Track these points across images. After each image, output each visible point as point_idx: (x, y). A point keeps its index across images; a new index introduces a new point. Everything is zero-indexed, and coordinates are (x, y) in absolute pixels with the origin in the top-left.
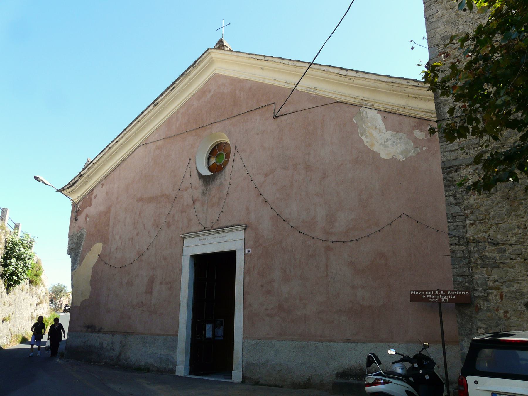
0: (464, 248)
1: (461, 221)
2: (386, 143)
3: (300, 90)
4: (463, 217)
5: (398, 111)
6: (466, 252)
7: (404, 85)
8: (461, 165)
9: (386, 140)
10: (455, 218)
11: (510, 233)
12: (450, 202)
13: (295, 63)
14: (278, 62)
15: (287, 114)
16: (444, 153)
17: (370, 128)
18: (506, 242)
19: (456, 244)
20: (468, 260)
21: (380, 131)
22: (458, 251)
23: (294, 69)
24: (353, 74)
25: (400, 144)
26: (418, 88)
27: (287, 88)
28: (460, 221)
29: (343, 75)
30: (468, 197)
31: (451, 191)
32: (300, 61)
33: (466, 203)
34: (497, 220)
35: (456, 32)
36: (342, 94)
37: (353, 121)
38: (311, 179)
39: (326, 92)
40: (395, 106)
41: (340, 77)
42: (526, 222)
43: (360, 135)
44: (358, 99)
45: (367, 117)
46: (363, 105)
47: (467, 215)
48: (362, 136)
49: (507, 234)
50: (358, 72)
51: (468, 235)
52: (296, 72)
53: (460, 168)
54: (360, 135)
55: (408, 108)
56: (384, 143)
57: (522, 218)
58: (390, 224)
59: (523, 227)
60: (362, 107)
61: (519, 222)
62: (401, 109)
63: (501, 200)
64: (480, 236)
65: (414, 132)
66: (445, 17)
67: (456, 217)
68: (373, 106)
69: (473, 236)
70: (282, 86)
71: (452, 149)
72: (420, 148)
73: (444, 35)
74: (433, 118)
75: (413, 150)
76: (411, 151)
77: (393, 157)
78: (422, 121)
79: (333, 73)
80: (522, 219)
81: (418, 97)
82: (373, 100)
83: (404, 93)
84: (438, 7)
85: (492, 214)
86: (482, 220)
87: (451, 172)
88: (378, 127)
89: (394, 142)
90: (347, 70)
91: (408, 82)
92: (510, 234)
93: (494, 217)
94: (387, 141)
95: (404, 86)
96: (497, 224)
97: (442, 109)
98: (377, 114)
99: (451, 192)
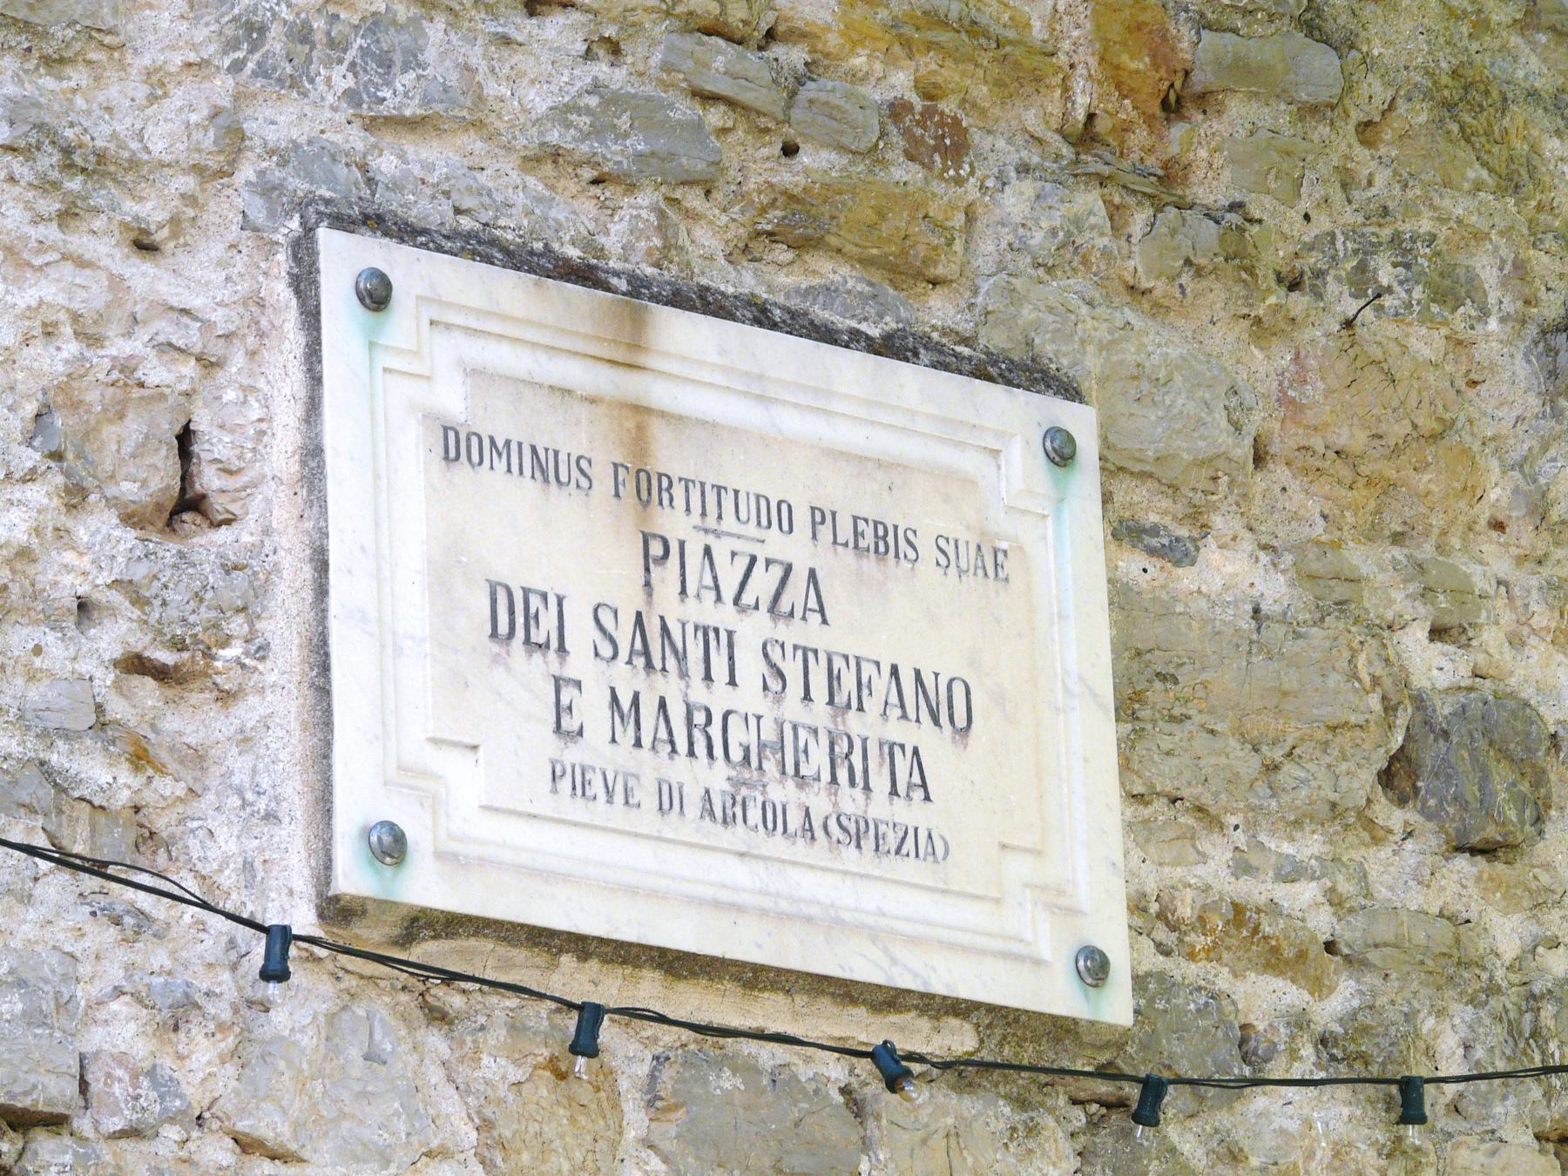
42: (209, 364)
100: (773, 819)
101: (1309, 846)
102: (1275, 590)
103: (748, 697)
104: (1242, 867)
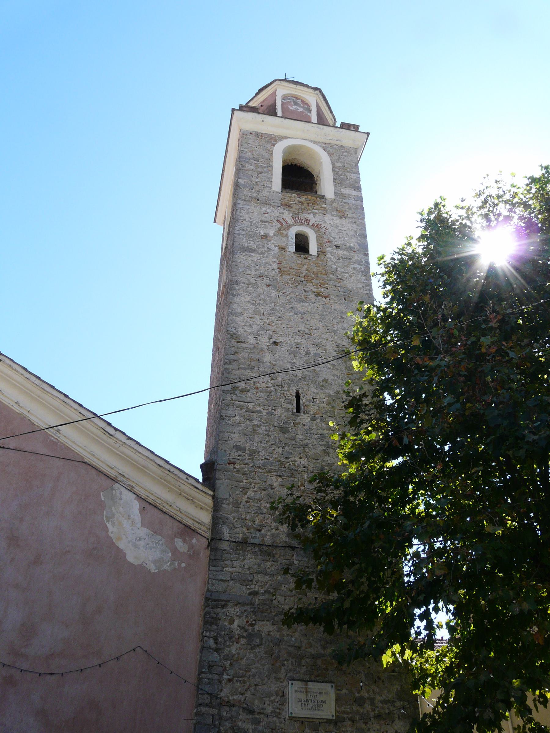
0: (215, 711)
1: (218, 674)
2: (138, 543)
3: (35, 423)
4: (221, 669)
5: (162, 507)
6: (217, 717)
7: (182, 479)
8: (229, 601)
9: (138, 539)
10: (211, 667)
11: (268, 699)
12: (210, 645)
13: (45, 386)
14: (17, 372)
15: (4, 448)
16: (214, 581)
17: (121, 514)
18: (262, 711)
19: (207, 705)
20: (217, 730)
21: (133, 523)
22: (207, 715)
23: (39, 392)
24: (124, 439)
25: (155, 550)
26: (196, 490)
27: (15, 411)
28: (216, 674)
29: (109, 434)
30: (231, 644)
31: (212, 631)
32: (53, 387)
33: (226, 651)
34: (257, 680)
35: (250, 447)
36: (96, 456)
37: (100, 496)
38: (12, 560)
39: (73, 442)
40: (160, 499)
41: (102, 434)
42: (285, 688)
43: (105, 519)
44: (115, 470)
45: (121, 499)
46: (119, 481)
47: (225, 667)
48: (108, 521)
49: (265, 701)
50: (129, 438)
51: (222, 694)
52: (39, 397)
53: (227, 605)
54: (105, 519)
55: (175, 507)
56: (135, 541)
57: (282, 682)
58: (118, 658)
59: (281, 694)
60: (117, 483)
61: (278, 687)
62: (167, 507)
63: (265, 656)
64: (235, 697)
65: (176, 540)
66: (243, 425)
67: (212, 666)
68: (133, 487)
69: (228, 697)
70: (9, 405)
71: (223, 579)
72: (178, 562)
73: (237, 445)
74: (201, 531)
75: (170, 563)
76: (166, 563)
77: (142, 564)
78: (187, 529)
79: (97, 425)
80: (281, 684)
81: (191, 500)
82: (135, 481)
83: (177, 488)
84: (236, 411)
85: (254, 671)
86: (241, 677)
87: (217, 607)
88: (132, 517)
89: (148, 544)
90: (116, 429)
91: (187, 478)
92: (267, 700)
93: (254, 676)
94: (140, 539)
95: (181, 481)
96: (256, 685)
97: (220, 526)
98: (135, 499)
99: (212, 633)
100: (314, 709)
101: (349, 707)
102: (347, 692)
103: (312, 703)
104: (344, 708)
